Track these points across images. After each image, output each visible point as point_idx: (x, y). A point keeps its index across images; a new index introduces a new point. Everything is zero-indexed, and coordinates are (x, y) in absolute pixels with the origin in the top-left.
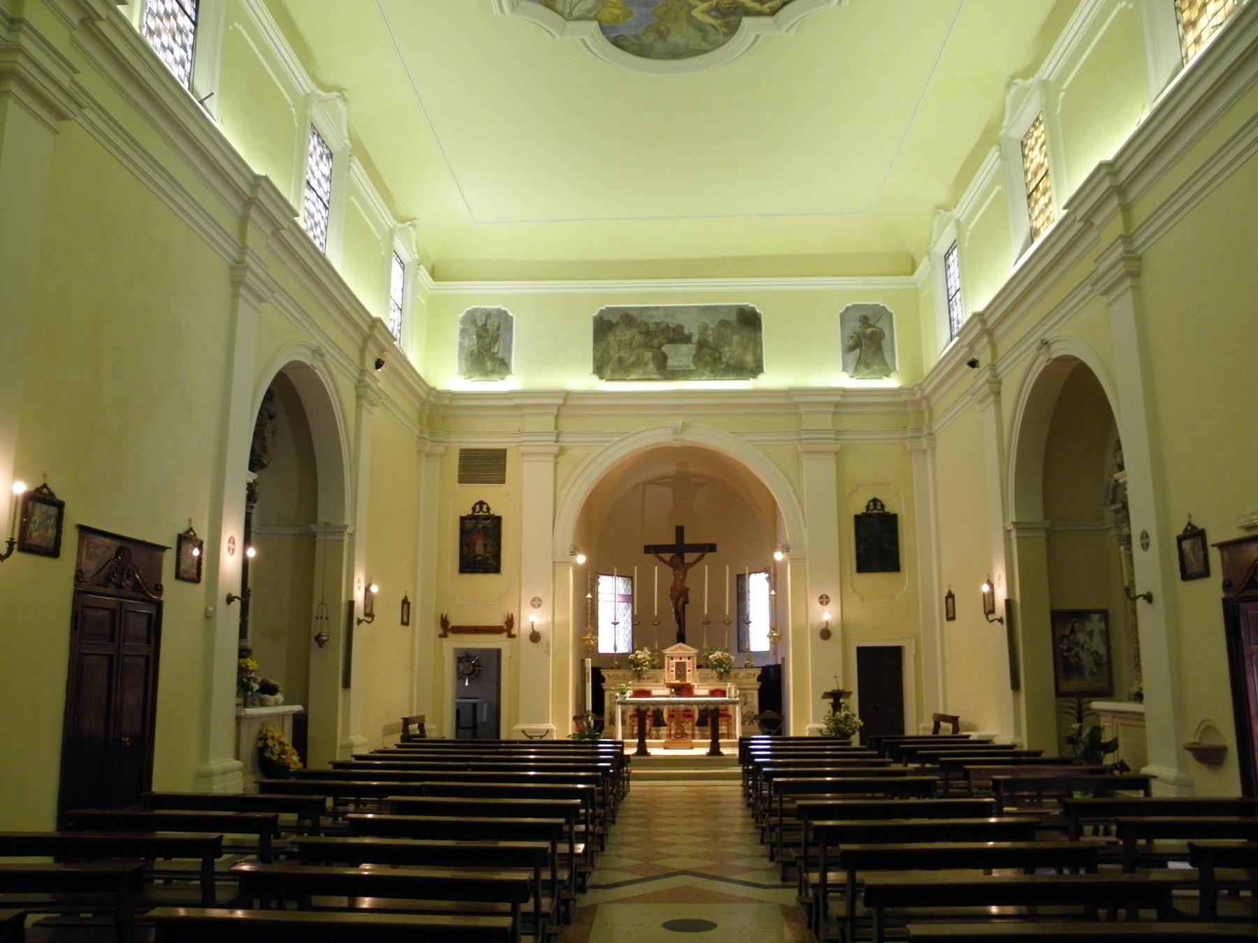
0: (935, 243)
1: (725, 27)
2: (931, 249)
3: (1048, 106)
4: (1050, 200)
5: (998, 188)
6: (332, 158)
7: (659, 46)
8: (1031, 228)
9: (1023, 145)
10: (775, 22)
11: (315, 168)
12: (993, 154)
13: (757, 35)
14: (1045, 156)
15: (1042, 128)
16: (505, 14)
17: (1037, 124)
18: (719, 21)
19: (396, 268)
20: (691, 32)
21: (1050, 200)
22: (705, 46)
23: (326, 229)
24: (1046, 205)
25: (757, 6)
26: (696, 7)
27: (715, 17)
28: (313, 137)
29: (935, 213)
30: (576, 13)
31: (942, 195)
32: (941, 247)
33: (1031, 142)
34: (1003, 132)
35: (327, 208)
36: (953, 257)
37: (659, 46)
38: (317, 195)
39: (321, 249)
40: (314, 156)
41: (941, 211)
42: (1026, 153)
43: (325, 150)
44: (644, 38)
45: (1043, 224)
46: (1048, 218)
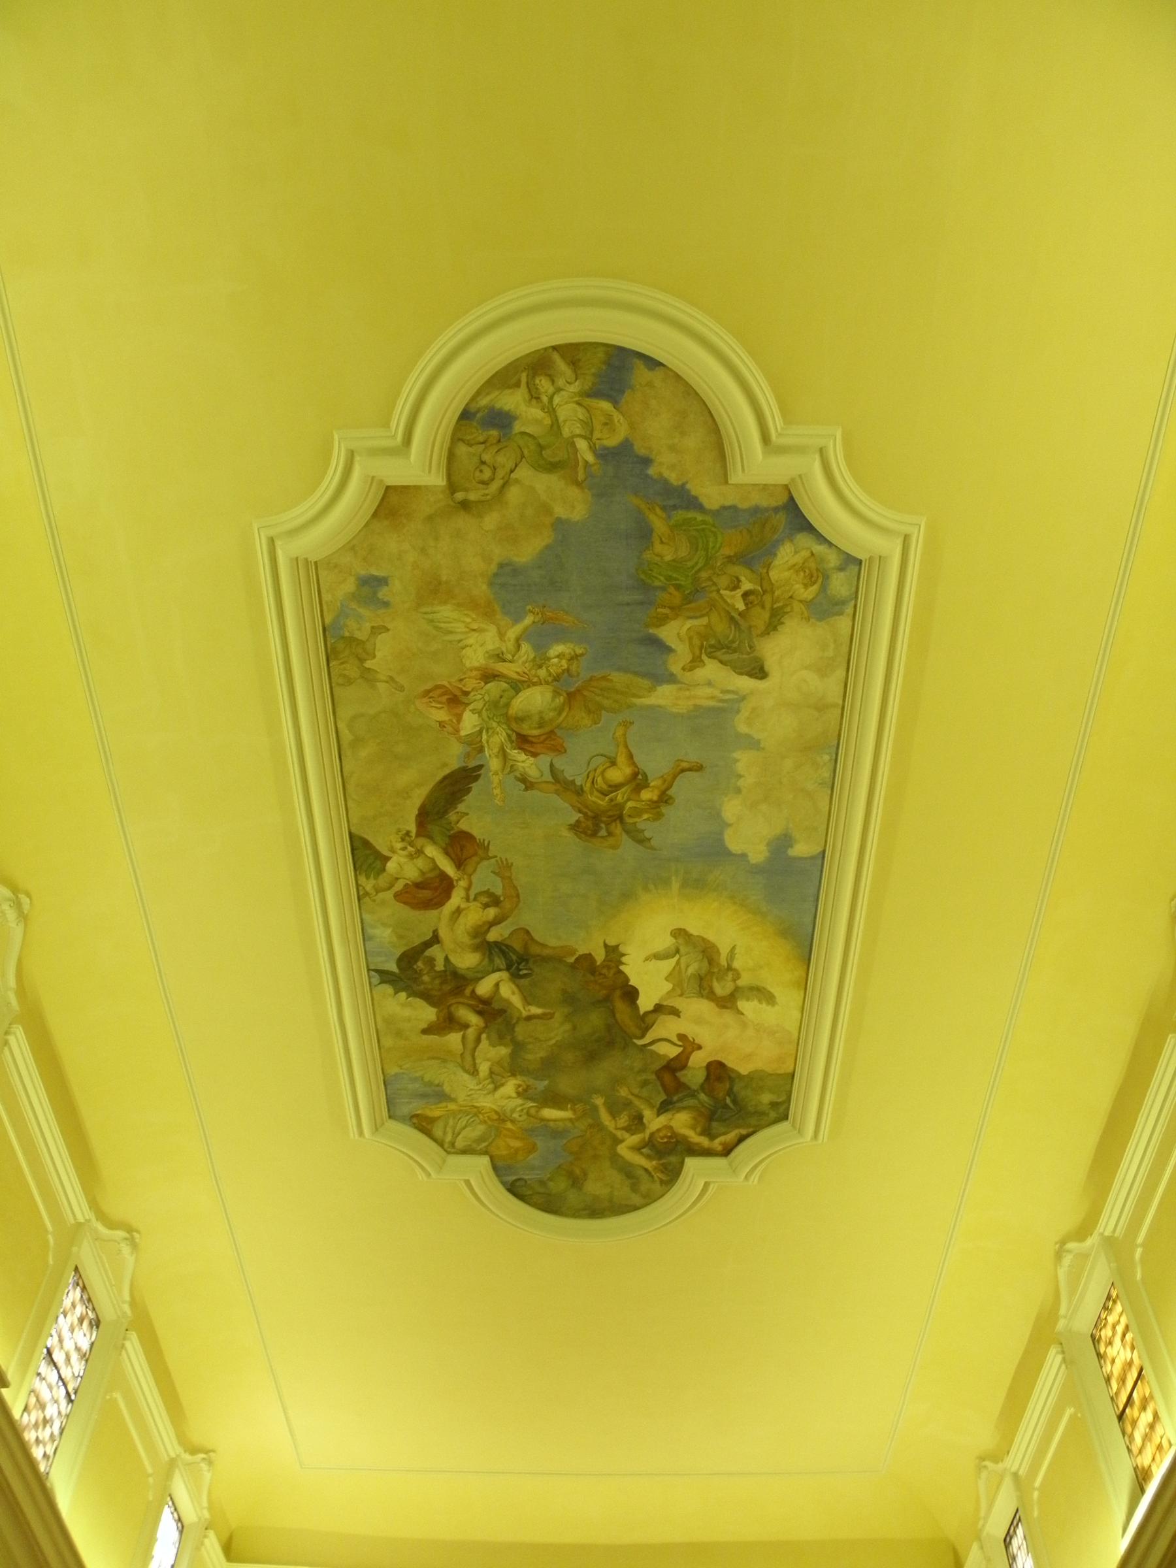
0: (986, 1518)
1: (662, 1172)
2: (981, 1530)
3: (1122, 1273)
4: (1156, 1416)
5: (1069, 1411)
6: (98, 1327)
7: (573, 1197)
8: (1136, 1468)
9: (1095, 1340)
10: (730, 1164)
11: (66, 1334)
12: (1053, 1359)
13: (706, 1183)
14: (1133, 1348)
15: (1119, 1308)
16: (364, 1137)
17: (1111, 1303)
18: (654, 1163)
19: (167, 1528)
20: (615, 1177)
21: (1156, 1416)
22: (636, 1199)
23: (61, 1434)
24: (1152, 1426)
25: (704, 1141)
26: (622, 1141)
27: (648, 1157)
28: (75, 1289)
29: (980, 1468)
30: (460, 1143)
31: (984, 1437)
32: (997, 1526)
33: (1106, 1333)
34: (1061, 1324)
35: (70, 1401)
36: (1018, 1541)
37: (573, 1197)
38: (60, 1377)
39: (42, 1467)
40: (69, 1316)
41: (987, 1463)
42: (1102, 1351)
43: (90, 1313)
44: (551, 1184)
45: (1153, 1459)
46: (1160, 1447)
